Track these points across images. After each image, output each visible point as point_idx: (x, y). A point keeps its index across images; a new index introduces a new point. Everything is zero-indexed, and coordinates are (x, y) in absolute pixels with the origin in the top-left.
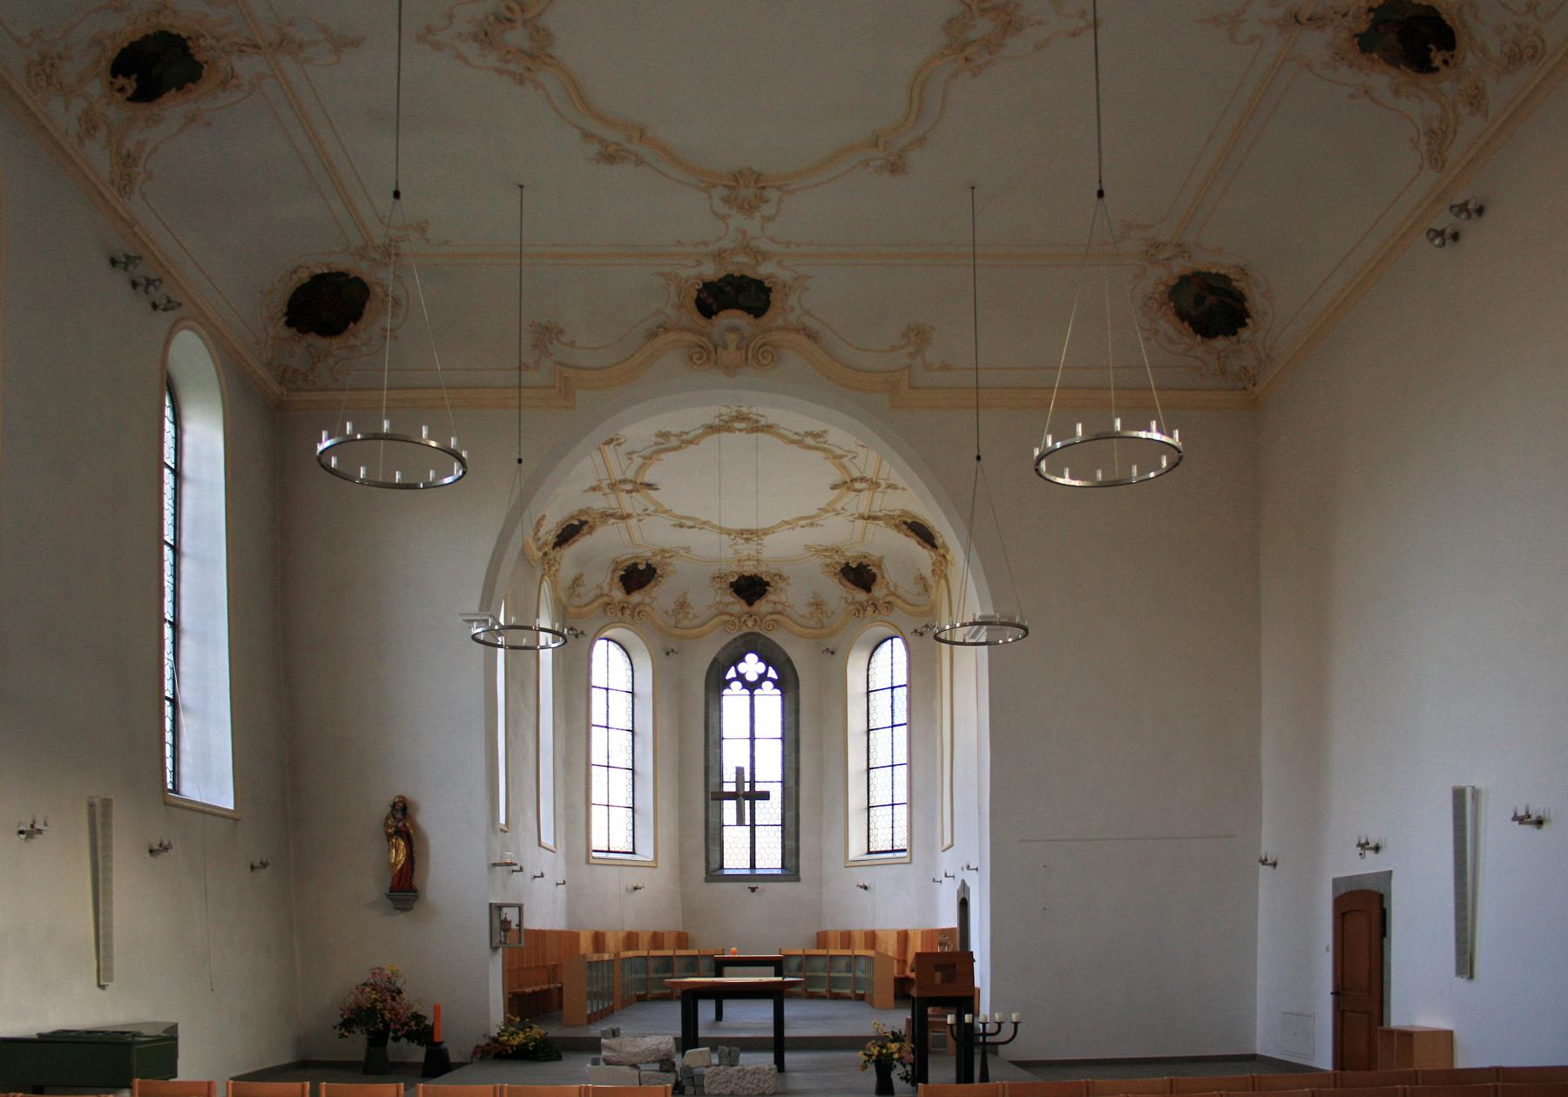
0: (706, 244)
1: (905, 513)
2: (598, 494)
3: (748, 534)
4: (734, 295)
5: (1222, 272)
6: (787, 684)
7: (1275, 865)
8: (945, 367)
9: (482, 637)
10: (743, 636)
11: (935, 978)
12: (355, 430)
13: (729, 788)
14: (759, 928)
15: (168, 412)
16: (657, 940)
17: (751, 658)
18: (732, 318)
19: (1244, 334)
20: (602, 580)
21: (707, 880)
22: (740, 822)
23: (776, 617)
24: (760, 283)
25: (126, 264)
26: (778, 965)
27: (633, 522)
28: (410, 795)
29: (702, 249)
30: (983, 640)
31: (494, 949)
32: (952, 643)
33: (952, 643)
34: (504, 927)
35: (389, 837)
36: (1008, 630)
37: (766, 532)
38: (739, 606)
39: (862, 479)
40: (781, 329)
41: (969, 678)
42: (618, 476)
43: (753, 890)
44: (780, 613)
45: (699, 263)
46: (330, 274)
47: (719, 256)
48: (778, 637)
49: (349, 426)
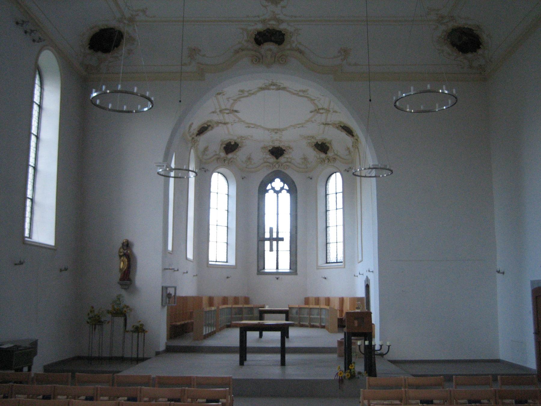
0: (259, 17)
1: (341, 122)
2: (215, 115)
3: (277, 131)
4: (270, 37)
5: (469, 27)
6: (293, 191)
7: (503, 273)
8: (356, 64)
9: (162, 173)
10: (274, 171)
11: (355, 323)
12: (106, 89)
13: (267, 235)
14: (277, 298)
15: (37, 81)
16: (236, 300)
17: (277, 180)
18: (269, 46)
19: (480, 52)
20: (216, 148)
21: (258, 274)
22: (271, 250)
23: (288, 164)
24: (280, 32)
25: (22, 25)
26: (286, 313)
27: (229, 125)
28: (130, 239)
29: (257, 19)
30: (373, 175)
31: (163, 306)
32: (361, 176)
33: (361, 176)
34: (168, 297)
35: (121, 256)
36: (384, 171)
37: (285, 129)
38: (272, 159)
39: (323, 109)
40: (289, 49)
41: (369, 189)
42: (223, 107)
43: (277, 279)
44: (290, 162)
45: (256, 24)
46: (107, 29)
47: (264, 22)
48: (289, 172)
49: (104, 87)
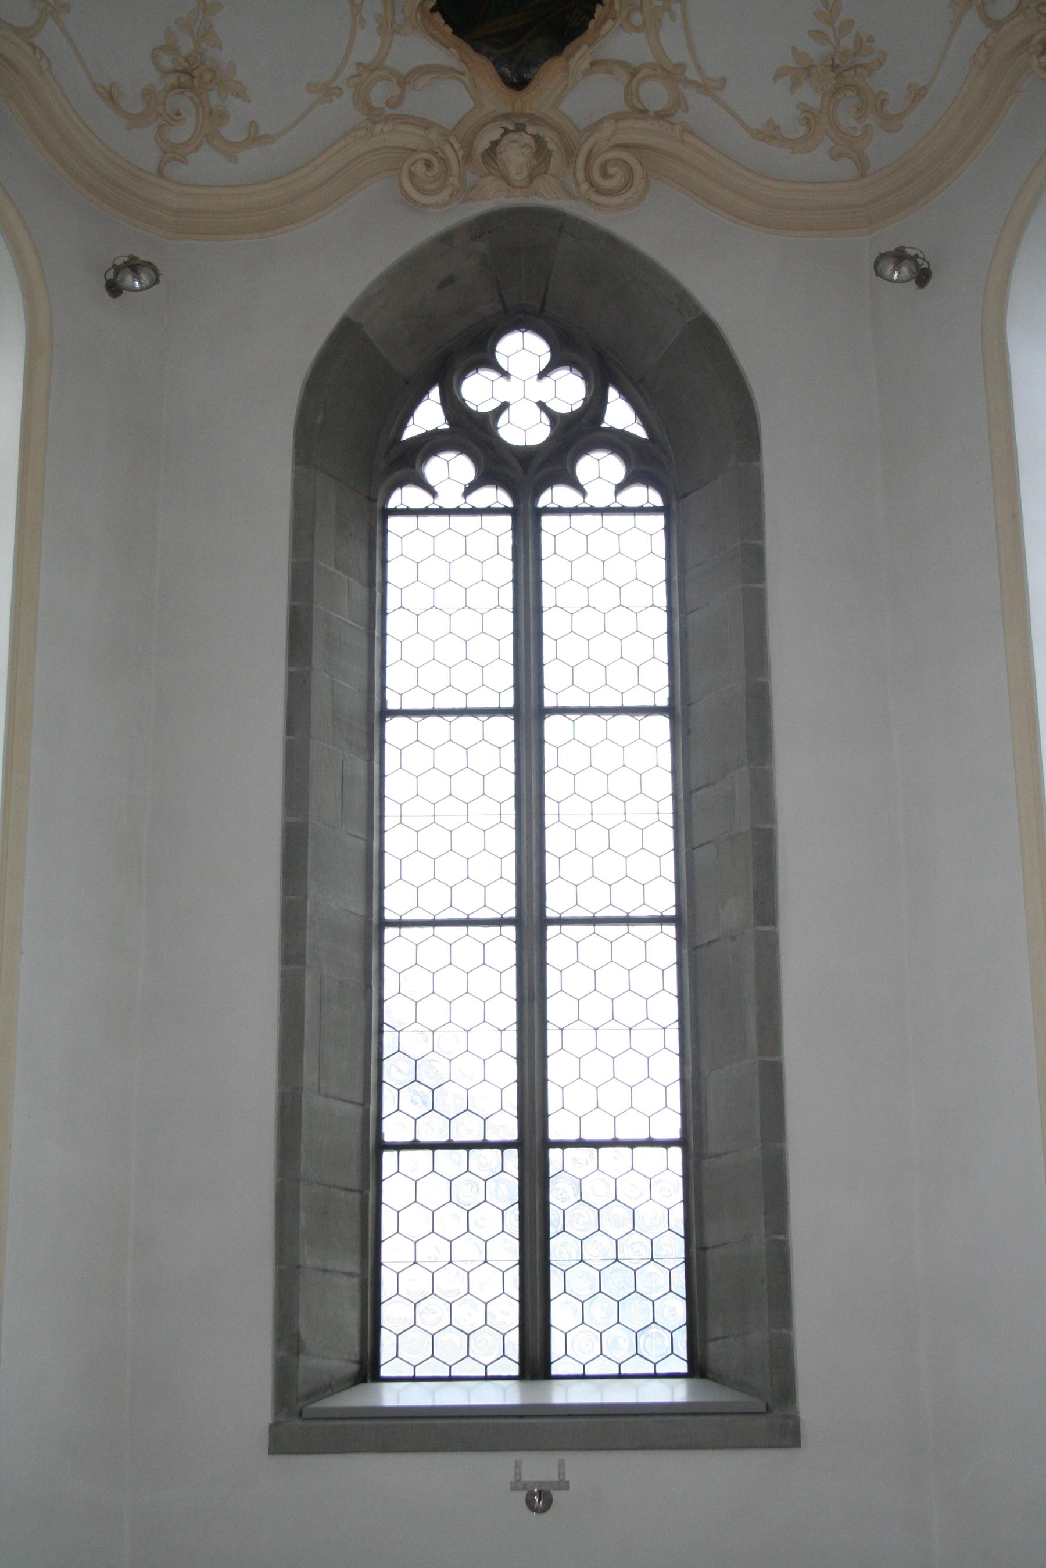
6: (699, 451)
17: (522, 350)
21: (281, 1443)
